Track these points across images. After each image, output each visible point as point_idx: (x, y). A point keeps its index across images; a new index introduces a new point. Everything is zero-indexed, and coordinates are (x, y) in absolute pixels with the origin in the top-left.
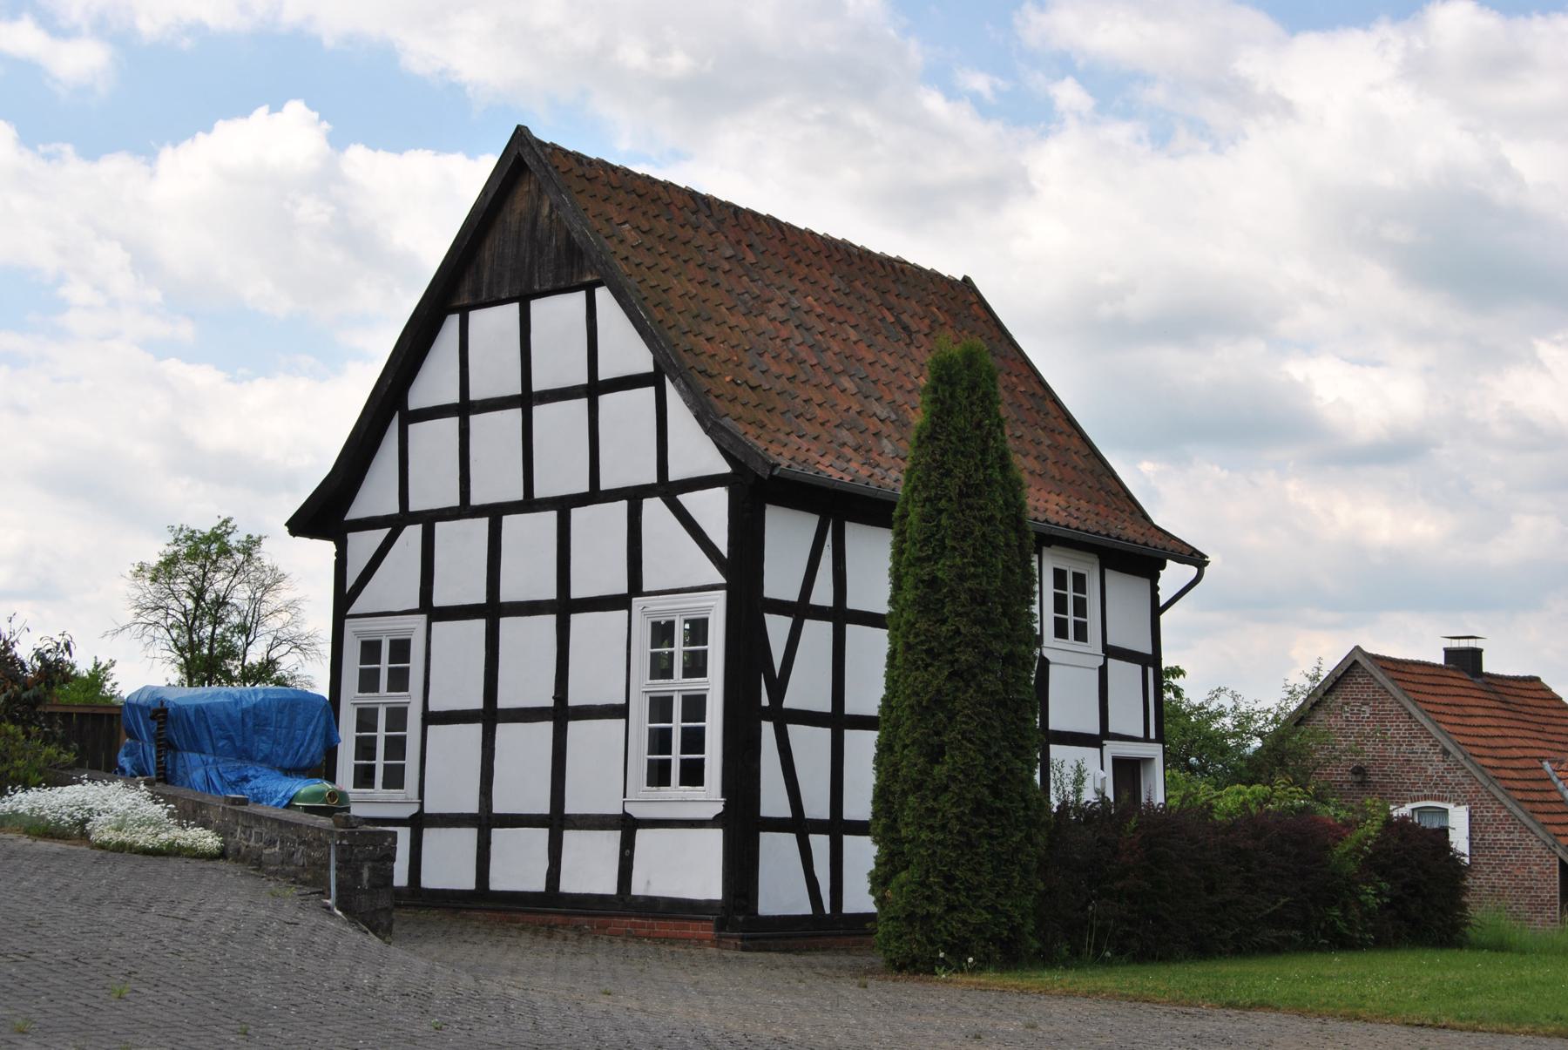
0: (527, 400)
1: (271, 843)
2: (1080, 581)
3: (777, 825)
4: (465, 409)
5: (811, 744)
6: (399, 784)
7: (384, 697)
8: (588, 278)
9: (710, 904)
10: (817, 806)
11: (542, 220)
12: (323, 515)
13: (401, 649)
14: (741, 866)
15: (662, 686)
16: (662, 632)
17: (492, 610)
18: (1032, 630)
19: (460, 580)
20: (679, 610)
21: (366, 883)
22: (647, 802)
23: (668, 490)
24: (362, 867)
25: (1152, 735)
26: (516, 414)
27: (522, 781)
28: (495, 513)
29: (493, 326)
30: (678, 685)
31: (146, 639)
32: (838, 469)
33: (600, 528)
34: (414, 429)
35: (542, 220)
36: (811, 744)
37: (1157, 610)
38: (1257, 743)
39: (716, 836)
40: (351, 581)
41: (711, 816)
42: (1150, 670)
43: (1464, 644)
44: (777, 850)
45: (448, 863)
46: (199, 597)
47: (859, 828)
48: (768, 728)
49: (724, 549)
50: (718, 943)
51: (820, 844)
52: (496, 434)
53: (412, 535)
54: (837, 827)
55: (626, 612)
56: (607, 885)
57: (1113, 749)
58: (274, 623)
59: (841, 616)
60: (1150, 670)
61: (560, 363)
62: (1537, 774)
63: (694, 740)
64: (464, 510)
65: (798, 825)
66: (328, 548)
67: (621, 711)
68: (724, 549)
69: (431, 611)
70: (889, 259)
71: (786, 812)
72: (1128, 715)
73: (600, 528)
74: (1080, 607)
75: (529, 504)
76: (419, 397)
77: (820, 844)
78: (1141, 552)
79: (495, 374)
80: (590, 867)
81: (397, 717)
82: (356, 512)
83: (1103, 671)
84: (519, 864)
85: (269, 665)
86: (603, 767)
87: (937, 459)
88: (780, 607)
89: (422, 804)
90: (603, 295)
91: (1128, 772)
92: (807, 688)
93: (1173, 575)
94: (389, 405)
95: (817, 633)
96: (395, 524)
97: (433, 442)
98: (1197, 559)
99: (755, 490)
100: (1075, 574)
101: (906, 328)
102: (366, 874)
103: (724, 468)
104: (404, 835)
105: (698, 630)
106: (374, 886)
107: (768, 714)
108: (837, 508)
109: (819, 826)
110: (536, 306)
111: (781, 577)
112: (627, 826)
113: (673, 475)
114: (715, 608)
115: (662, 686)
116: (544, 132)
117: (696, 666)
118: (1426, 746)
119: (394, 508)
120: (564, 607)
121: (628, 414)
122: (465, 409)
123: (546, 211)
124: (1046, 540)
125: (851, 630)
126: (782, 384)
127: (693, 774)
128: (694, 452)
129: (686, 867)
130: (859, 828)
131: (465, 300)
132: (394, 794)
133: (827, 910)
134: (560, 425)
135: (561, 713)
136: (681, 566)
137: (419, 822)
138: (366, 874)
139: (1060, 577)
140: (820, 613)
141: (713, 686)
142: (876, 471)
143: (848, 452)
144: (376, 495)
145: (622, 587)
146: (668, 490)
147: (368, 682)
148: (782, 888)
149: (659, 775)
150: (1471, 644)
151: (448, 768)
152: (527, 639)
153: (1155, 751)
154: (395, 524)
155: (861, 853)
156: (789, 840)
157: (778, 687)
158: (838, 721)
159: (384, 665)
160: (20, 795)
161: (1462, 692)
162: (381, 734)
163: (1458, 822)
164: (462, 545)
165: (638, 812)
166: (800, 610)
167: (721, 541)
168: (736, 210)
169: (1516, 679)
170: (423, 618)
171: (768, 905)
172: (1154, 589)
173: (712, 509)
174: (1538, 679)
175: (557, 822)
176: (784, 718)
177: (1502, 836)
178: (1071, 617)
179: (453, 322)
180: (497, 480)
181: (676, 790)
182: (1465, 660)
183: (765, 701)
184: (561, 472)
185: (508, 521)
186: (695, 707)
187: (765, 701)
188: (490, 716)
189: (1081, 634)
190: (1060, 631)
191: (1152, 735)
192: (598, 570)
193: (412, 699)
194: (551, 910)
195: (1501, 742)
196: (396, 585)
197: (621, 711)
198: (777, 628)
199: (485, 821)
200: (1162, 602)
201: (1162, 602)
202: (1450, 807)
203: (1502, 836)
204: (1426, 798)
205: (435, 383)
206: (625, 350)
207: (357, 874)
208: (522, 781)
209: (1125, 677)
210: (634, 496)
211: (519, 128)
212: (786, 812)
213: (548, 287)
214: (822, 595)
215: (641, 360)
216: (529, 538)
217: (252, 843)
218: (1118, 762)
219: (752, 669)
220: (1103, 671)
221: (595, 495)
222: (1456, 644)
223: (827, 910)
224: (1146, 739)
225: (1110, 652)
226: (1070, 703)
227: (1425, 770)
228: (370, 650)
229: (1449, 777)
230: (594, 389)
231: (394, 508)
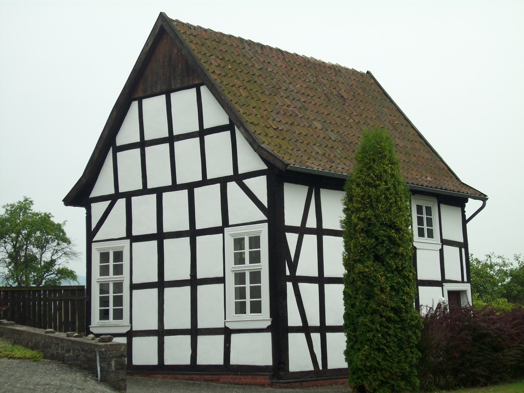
4: (142, 144)
13: (118, 256)
16: (239, 243)
17: (160, 236)
19: (145, 224)
23: (238, 178)
25: (465, 280)
29: (154, 105)
33: (208, 198)
41: (265, 327)
49: (265, 204)
52: (157, 155)
53: (121, 203)
55: (222, 235)
57: (448, 287)
66: (82, 211)
67: (221, 280)
68: (265, 204)
73: (208, 198)
82: (95, 193)
83: (441, 251)
88: (293, 229)
89: (131, 326)
94: (108, 144)
97: (129, 160)
103: (265, 167)
107: (289, 279)
116: (172, 15)
117: (255, 258)
120: (193, 233)
122: (142, 144)
128: (249, 161)
136: (244, 209)
141: (264, 266)
144: (104, 186)
146: (238, 178)
157: (294, 266)
167: (264, 201)
170: (129, 240)
173: (259, 186)
176: (297, 280)
179: (135, 105)
183: (288, 273)
186: (256, 276)
187: (288, 273)
189: (431, 234)
191: (465, 280)
192: (208, 215)
197: (221, 280)
198: (292, 239)
205: (128, 133)
206: (216, 115)
210: (223, 181)
211: (161, 13)
220: (441, 251)
221: (205, 182)
225: (444, 242)
228: (104, 257)
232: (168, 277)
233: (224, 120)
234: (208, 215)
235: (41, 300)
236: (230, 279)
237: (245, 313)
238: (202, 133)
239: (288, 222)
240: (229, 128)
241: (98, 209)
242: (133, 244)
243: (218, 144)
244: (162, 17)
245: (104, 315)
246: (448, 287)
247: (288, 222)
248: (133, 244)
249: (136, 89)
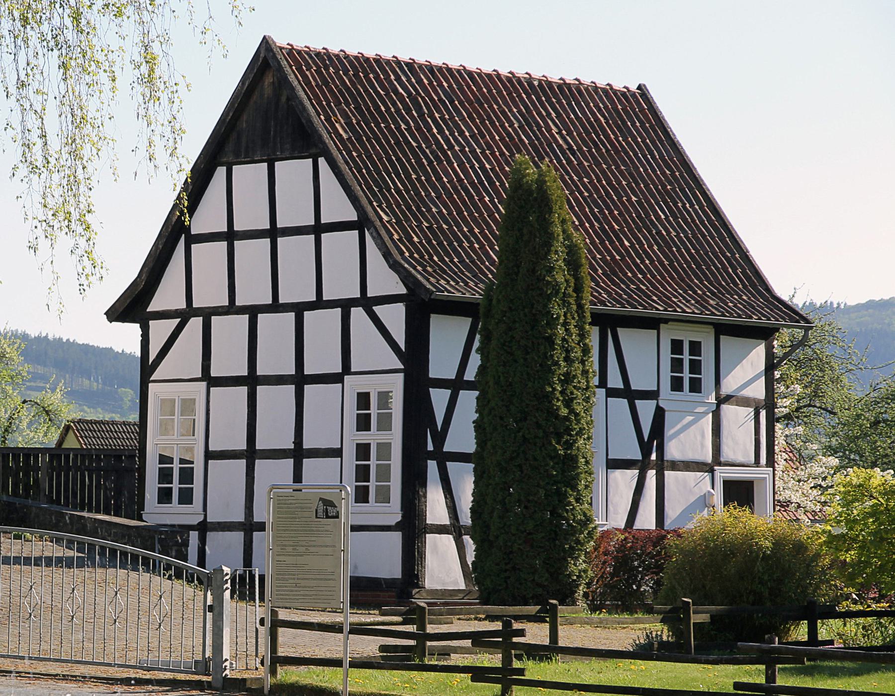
2: (695, 348)
3: (440, 530)
4: (231, 236)
6: (674, 342)
9: (394, 580)
16: (363, 400)
17: (252, 381)
18: (553, 413)
19: (229, 359)
20: (373, 385)
23: (367, 303)
24: (171, 550)
29: (249, 177)
30: (372, 437)
33: (323, 326)
40: (152, 357)
41: (393, 523)
42: (763, 414)
49: (402, 346)
52: (252, 255)
53: (195, 324)
55: (340, 385)
61: (295, 210)
66: (135, 329)
67: (337, 453)
68: (402, 346)
71: (445, 520)
73: (323, 326)
74: (695, 367)
79: (251, 214)
82: (154, 306)
88: (441, 383)
89: (206, 516)
94: (175, 234)
97: (209, 259)
100: (691, 342)
103: (404, 291)
104: (194, 536)
107: (431, 456)
113: (370, 294)
114: (396, 385)
116: (281, 40)
117: (385, 423)
120: (300, 380)
122: (231, 236)
127: (384, 496)
128: (384, 281)
131: (231, 159)
136: (373, 351)
141: (395, 437)
144: (168, 295)
146: (367, 303)
152: (276, 402)
157: (440, 438)
164: (230, 332)
167: (401, 339)
170: (204, 383)
173: (395, 317)
176: (443, 458)
179: (221, 172)
183: (430, 447)
185: (263, 319)
186: (384, 450)
187: (430, 447)
189: (696, 386)
192: (322, 357)
196: (185, 357)
197: (337, 453)
198: (439, 398)
206: (338, 206)
210: (346, 305)
211: (264, 37)
212: (445, 520)
216: (276, 330)
221: (320, 304)
232: (261, 444)
233: (352, 215)
234: (322, 357)
235: (69, 469)
236: (350, 453)
237: (368, 502)
238: (318, 229)
239: (434, 372)
240: (361, 225)
241: (160, 330)
242: (211, 389)
243: (341, 248)
244: (266, 44)
245: (165, 496)
246: (722, 473)
247: (434, 372)
248: (211, 389)
249: (226, 147)
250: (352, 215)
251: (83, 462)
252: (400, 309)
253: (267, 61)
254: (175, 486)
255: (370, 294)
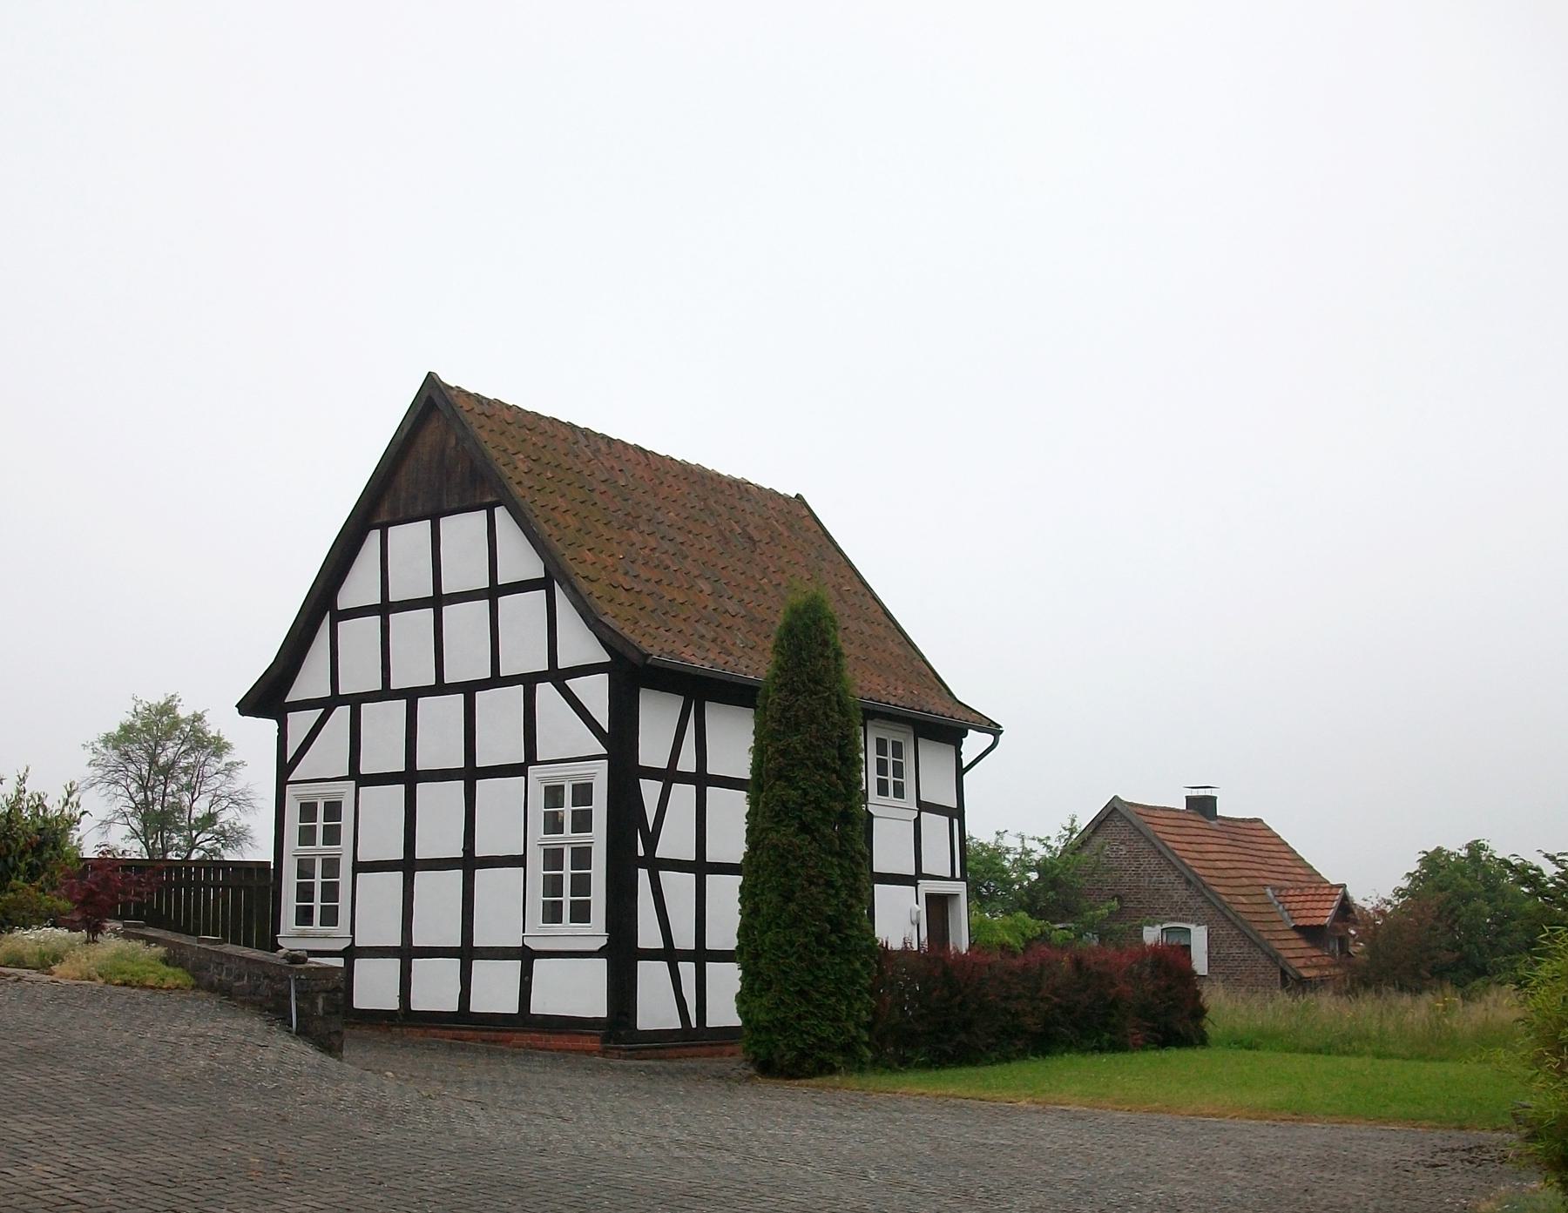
0: (437, 601)
1: (239, 977)
4: (385, 609)
5: (678, 886)
7: (320, 847)
8: (489, 499)
9: (596, 1021)
10: (684, 939)
11: (446, 455)
12: (267, 698)
13: (333, 810)
14: (622, 990)
15: (554, 839)
16: (553, 795)
17: (410, 777)
19: (383, 754)
21: (319, 1009)
22: (542, 935)
23: (558, 676)
25: (958, 875)
26: (428, 613)
27: (437, 918)
28: (412, 696)
29: (409, 539)
31: (111, 796)
32: (700, 659)
34: (342, 626)
35: (446, 455)
36: (678, 886)
37: (961, 771)
38: (1034, 876)
39: (601, 964)
42: (956, 822)
43: (1202, 792)
44: (652, 979)
45: (374, 986)
46: (153, 761)
47: (722, 956)
48: (643, 875)
50: (604, 1053)
51: (687, 969)
52: (412, 628)
53: (342, 713)
54: (702, 955)
56: (508, 1004)
57: (926, 886)
58: (215, 782)
59: (702, 780)
60: (956, 822)
61: (466, 570)
62: (1258, 899)
63: (582, 885)
64: (386, 693)
65: (669, 954)
66: (272, 725)
67: (519, 861)
69: (358, 777)
70: (735, 480)
72: (938, 859)
73: (500, 713)
74: (899, 771)
75: (440, 688)
76: (345, 601)
77: (687, 969)
78: (946, 724)
79: (411, 580)
80: (495, 990)
81: (331, 866)
83: (917, 822)
84: (436, 987)
85: (210, 818)
86: (505, 910)
87: (745, 639)
88: (653, 773)
90: (501, 513)
91: (938, 906)
92: (675, 841)
93: (974, 743)
94: (322, 605)
95: (683, 795)
96: (327, 705)
97: (359, 636)
98: (995, 730)
99: (631, 675)
101: (750, 538)
102: (320, 1002)
105: (583, 793)
106: (326, 1013)
108: (699, 691)
109: (686, 955)
110: (446, 523)
111: (653, 749)
112: (526, 956)
113: (562, 664)
114: (599, 775)
115: (554, 839)
117: (582, 822)
118: (1172, 878)
119: (326, 692)
120: (471, 774)
121: (524, 612)
122: (385, 609)
123: (453, 442)
124: (872, 714)
125: (711, 791)
126: (651, 587)
127: (581, 913)
128: (579, 645)
129: (574, 990)
130: (722, 956)
131: (384, 518)
132: (579, 928)
133: (694, 1025)
134: (467, 621)
135: (469, 863)
136: (566, 736)
137: (352, 953)
138: (320, 1002)
139: (881, 744)
140: (685, 778)
142: (730, 659)
143: (707, 645)
144: (311, 682)
145: (520, 758)
146: (558, 676)
147: (307, 836)
148: (656, 1007)
149: (552, 913)
150: (1208, 792)
151: (375, 909)
153: (960, 888)
154: (327, 705)
155: (725, 981)
156: (662, 967)
157: (652, 840)
158: (701, 867)
159: (320, 823)
160: (18, 933)
161: (1200, 832)
162: (318, 881)
163: (1199, 939)
164: (384, 721)
165: (534, 945)
166: (669, 776)
167: (604, 721)
168: (610, 441)
169: (1243, 820)
171: (644, 1022)
172: (959, 754)
173: (595, 692)
174: (1260, 821)
175: (467, 953)
176: (657, 866)
177: (1234, 950)
178: (890, 778)
179: (375, 536)
180: (413, 669)
181: (566, 926)
182: (1202, 805)
183: (641, 852)
184: (467, 663)
185: (422, 702)
186: (582, 857)
187: (641, 852)
188: (409, 865)
189: (899, 792)
190: (883, 790)
191: (958, 875)
192: (500, 739)
193: (344, 850)
194: (463, 1025)
195: (1233, 873)
196: (329, 755)
197: (519, 861)
198: (650, 790)
199: (407, 953)
200: (965, 765)
201: (965, 765)
202: (1192, 927)
203: (1234, 950)
204: (1173, 920)
205: (360, 588)
206: (519, 560)
207: (314, 1004)
208: (437, 918)
209: (936, 827)
210: (529, 681)
212: (659, 944)
213: (454, 505)
214: (687, 763)
215: (533, 568)
217: (223, 977)
218: (930, 897)
219: (629, 824)
220: (917, 822)
221: (496, 680)
222: (1195, 793)
223: (694, 1025)
224: (953, 878)
225: (923, 806)
226: (890, 848)
227: (1171, 897)
228: (308, 811)
229: (1191, 903)
230: (494, 592)
231: (326, 692)
233: (536, 570)
236: (536, 860)
243: (523, 615)
244: (431, 379)
245: (304, 916)
247: (644, 761)
250: (536, 570)
251: (178, 875)
252: (601, 682)
253: (435, 404)
254: (317, 904)
255: (562, 664)
